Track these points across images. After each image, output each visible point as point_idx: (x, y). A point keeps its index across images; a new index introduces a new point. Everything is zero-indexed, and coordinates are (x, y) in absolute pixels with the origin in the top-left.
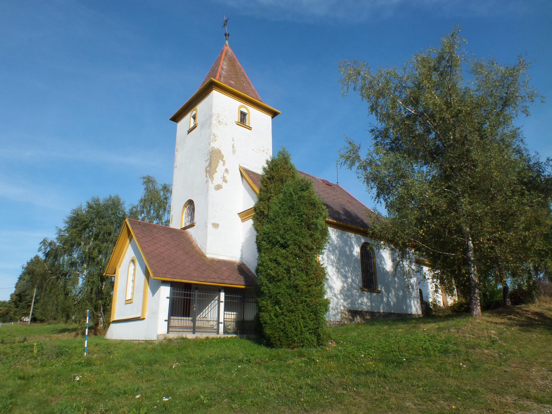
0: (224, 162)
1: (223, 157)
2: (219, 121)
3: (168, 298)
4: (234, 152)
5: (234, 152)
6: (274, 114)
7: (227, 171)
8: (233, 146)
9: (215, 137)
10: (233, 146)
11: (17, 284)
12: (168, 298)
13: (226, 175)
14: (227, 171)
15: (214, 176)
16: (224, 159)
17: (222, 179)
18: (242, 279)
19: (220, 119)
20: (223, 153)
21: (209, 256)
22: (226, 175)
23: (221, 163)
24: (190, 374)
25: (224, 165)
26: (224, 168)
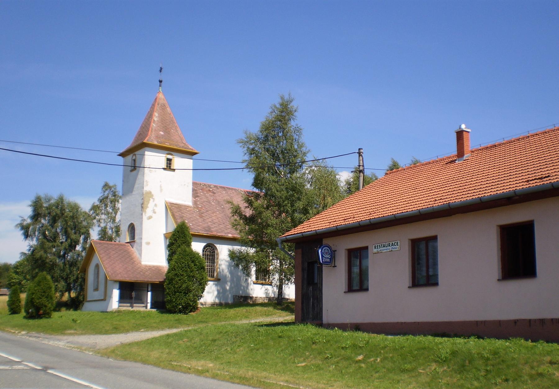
0: (153, 199)
4: (161, 190)
5: (161, 190)
7: (156, 205)
8: (161, 187)
10: (161, 187)
14: (156, 205)
23: (151, 200)
25: (154, 201)
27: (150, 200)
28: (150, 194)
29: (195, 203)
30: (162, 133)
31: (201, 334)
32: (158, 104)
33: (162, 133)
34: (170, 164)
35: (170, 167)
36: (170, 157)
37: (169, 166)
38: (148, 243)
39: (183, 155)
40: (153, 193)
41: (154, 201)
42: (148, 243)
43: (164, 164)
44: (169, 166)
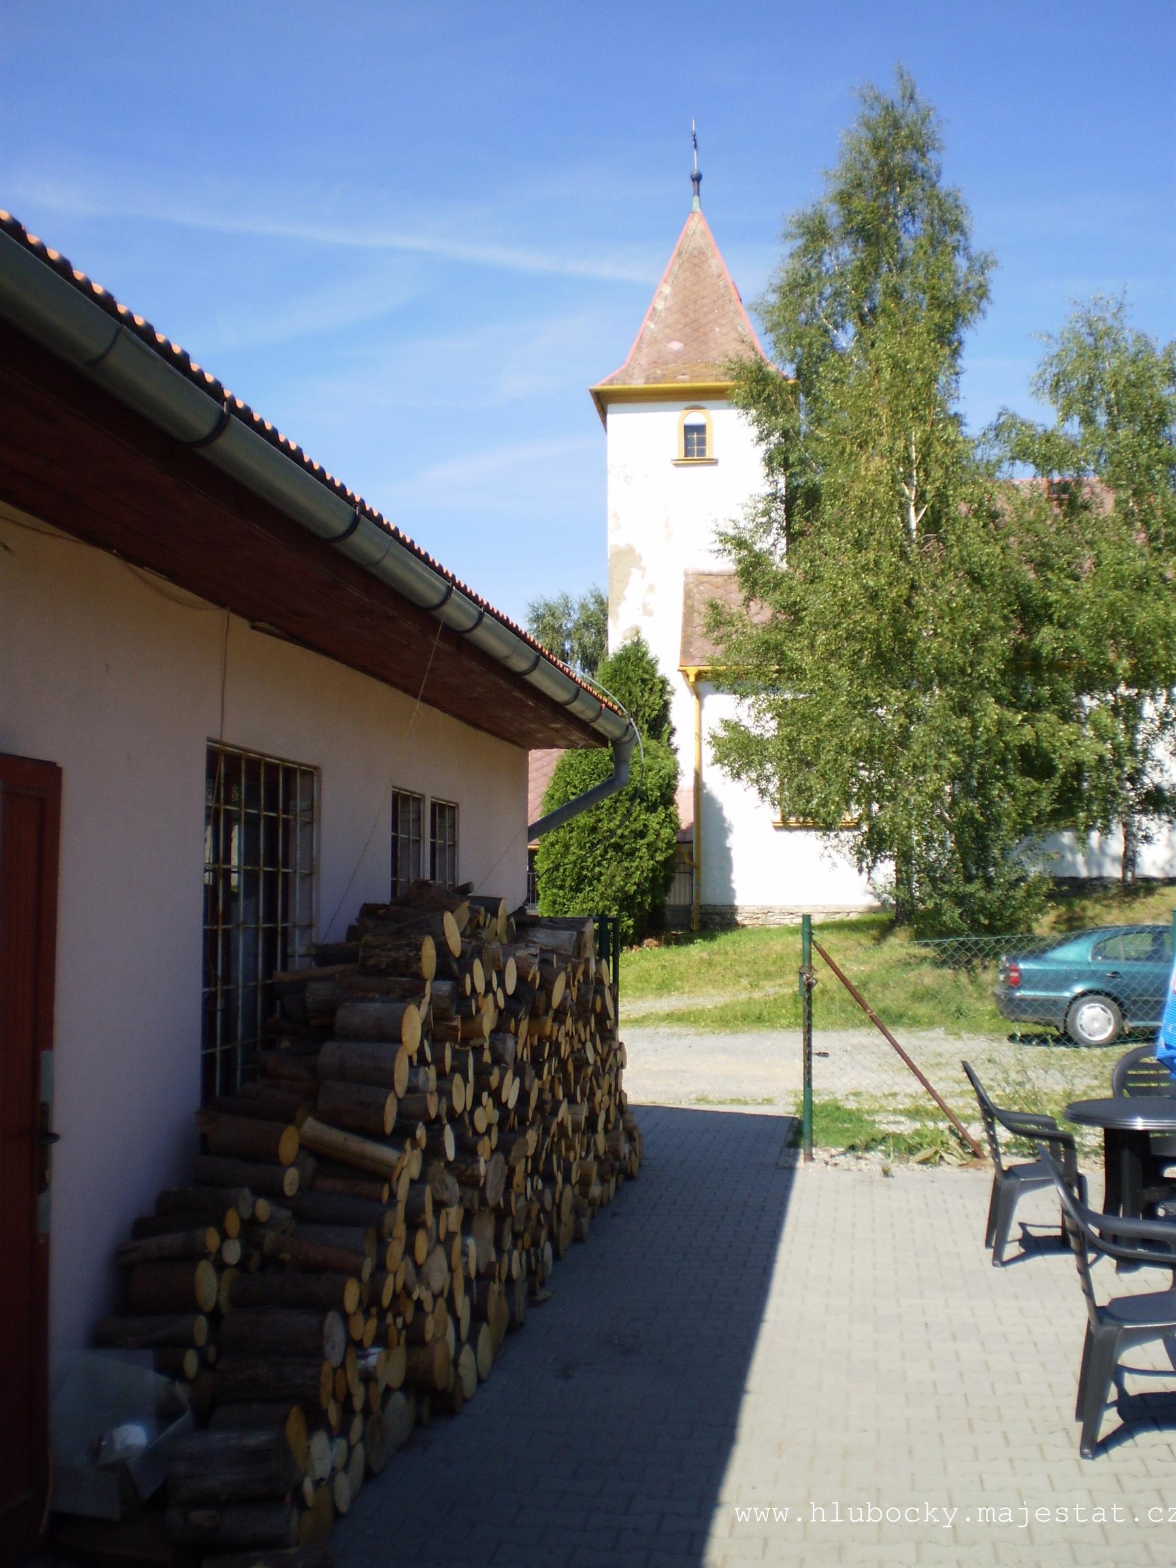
1: (640, 558)
11: (721, 809)
14: (651, 588)
23: (635, 573)
27: (629, 574)
33: (676, 346)
34: (702, 442)
35: (702, 452)
36: (695, 418)
43: (678, 450)
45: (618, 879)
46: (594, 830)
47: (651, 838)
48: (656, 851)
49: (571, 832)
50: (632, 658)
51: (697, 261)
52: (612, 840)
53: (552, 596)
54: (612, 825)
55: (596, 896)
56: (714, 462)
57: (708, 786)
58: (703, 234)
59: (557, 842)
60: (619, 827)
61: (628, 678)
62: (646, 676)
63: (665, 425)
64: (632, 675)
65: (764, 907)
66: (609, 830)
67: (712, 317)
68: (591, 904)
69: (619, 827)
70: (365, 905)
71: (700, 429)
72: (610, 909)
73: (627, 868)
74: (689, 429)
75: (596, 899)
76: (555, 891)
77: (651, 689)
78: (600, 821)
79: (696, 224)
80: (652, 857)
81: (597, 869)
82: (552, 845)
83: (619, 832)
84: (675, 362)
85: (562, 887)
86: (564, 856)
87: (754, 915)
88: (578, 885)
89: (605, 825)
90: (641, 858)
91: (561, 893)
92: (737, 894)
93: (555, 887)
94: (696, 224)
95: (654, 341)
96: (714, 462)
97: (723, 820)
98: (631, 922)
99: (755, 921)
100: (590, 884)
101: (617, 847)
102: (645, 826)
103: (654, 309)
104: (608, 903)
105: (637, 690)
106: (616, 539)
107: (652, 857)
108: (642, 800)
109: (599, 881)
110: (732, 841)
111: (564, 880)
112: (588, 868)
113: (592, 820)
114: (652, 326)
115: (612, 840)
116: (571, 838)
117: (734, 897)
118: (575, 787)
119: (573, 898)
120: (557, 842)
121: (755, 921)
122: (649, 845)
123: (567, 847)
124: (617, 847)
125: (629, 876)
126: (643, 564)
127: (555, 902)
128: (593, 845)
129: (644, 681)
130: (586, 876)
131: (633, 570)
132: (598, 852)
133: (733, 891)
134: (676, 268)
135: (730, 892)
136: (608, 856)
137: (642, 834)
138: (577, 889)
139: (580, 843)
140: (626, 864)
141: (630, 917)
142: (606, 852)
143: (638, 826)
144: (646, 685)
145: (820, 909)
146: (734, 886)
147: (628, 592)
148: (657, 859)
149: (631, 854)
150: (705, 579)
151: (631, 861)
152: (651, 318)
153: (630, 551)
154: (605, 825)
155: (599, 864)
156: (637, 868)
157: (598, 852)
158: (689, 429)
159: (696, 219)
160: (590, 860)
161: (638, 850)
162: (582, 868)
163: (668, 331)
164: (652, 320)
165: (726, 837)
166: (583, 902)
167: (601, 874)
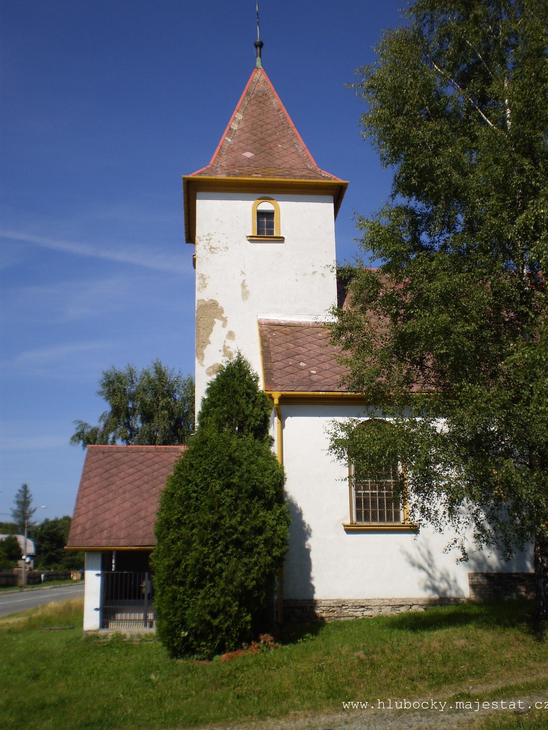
0: (225, 320)
1: (222, 311)
2: (211, 248)
3: (96, 609)
4: (245, 295)
5: (245, 295)
6: (336, 194)
7: (231, 335)
8: (243, 286)
9: (205, 279)
10: (243, 286)
11: (300, 514)
12: (96, 609)
13: (229, 343)
14: (231, 335)
15: (205, 351)
16: (224, 316)
17: (222, 353)
18: (33, 509)
19: (213, 243)
20: (221, 304)
21: (286, 421)
22: (229, 343)
23: (218, 323)
24: (187, 698)
25: (224, 326)
26: (225, 332)
27: (213, 323)
28: (213, 309)
29: (536, 570)
30: (248, 155)
31: (530, 345)
32: (248, 94)
33: (248, 155)
34: (271, 225)
35: (272, 232)
36: (266, 206)
37: (266, 228)
38: (220, 351)
39: (328, 408)
40: (221, 303)
41: (224, 326)
42: (220, 351)
43: (250, 228)
44: (266, 228)
45: (239, 574)
46: (216, 526)
47: (269, 534)
48: (273, 547)
49: (192, 529)
50: (238, 375)
51: (261, 99)
52: (235, 537)
53: (122, 369)
54: (234, 521)
55: (216, 591)
56: (281, 240)
57: (289, 494)
58: (265, 82)
59: (179, 539)
60: (240, 523)
61: (235, 392)
62: (249, 391)
63: (241, 211)
64: (239, 389)
65: (339, 601)
66: (231, 527)
67: (275, 137)
68: (213, 601)
69: (240, 523)
70: (310, 534)
71: (270, 215)
72: (230, 606)
73: (246, 564)
74: (261, 215)
75: (218, 595)
76: (174, 587)
77: (253, 402)
78: (221, 517)
79: (259, 76)
80: (269, 553)
81: (218, 565)
82: (174, 542)
83: (241, 528)
84: (248, 165)
85: (182, 584)
86: (185, 552)
87: (330, 608)
88: (199, 581)
89: (228, 522)
90: (259, 553)
91: (182, 589)
92: (316, 590)
93: (175, 583)
94: (259, 76)
95: (231, 150)
96: (281, 240)
97: (303, 524)
98: (249, 618)
99: (331, 614)
100: (212, 580)
101: (238, 543)
102: (264, 522)
103: (230, 129)
104: (229, 598)
105: (243, 401)
106: (202, 295)
107: (269, 553)
108: (260, 498)
109: (220, 577)
110: (312, 543)
111: (185, 577)
112: (210, 563)
113: (216, 517)
114: (230, 141)
115: (235, 537)
116: (192, 535)
117: (313, 592)
118: (197, 485)
119: (193, 594)
120: (179, 539)
121: (331, 614)
122: (266, 542)
123: (189, 543)
124: (238, 543)
125: (248, 571)
126: (224, 316)
127: (174, 599)
128: (216, 542)
129: (248, 395)
130: (208, 572)
131: (215, 320)
132: (219, 548)
133: (313, 587)
134: (246, 103)
135: (312, 589)
136: (229, 552)
137: (259, 531)
138: (199, 586)
139: (201, 541)
140: (246, 560)
141: (248, 612)
142: (227, 548)
143: (257, 523)
144: (250, 398)
145: (387, 602)
146: (314, 583)
147: (212, 338)
148: (274, 554)
149: (250, 551)
150: (276, 328)
151: (251, 557)
152: (228, 135)
153: (214, 304)
154: (228, 522)
155: (220, 560)
156: (255, 564)
157: (219, 548)
158: (261, 215)
159: (259, 72)
160: (212, 556)
161: (257, 546)
162: (205, 565)
163: (242, 145)
164: (229, 137)
165: (306, 539)
166: (203, 598)
167: (222, 571)
